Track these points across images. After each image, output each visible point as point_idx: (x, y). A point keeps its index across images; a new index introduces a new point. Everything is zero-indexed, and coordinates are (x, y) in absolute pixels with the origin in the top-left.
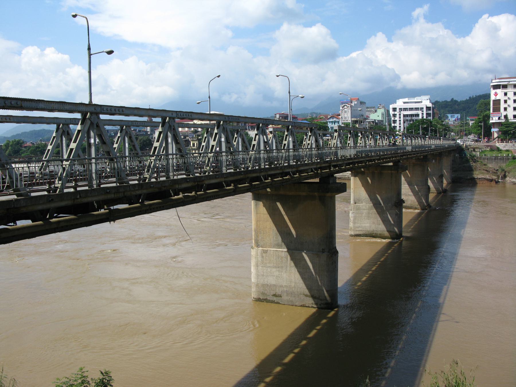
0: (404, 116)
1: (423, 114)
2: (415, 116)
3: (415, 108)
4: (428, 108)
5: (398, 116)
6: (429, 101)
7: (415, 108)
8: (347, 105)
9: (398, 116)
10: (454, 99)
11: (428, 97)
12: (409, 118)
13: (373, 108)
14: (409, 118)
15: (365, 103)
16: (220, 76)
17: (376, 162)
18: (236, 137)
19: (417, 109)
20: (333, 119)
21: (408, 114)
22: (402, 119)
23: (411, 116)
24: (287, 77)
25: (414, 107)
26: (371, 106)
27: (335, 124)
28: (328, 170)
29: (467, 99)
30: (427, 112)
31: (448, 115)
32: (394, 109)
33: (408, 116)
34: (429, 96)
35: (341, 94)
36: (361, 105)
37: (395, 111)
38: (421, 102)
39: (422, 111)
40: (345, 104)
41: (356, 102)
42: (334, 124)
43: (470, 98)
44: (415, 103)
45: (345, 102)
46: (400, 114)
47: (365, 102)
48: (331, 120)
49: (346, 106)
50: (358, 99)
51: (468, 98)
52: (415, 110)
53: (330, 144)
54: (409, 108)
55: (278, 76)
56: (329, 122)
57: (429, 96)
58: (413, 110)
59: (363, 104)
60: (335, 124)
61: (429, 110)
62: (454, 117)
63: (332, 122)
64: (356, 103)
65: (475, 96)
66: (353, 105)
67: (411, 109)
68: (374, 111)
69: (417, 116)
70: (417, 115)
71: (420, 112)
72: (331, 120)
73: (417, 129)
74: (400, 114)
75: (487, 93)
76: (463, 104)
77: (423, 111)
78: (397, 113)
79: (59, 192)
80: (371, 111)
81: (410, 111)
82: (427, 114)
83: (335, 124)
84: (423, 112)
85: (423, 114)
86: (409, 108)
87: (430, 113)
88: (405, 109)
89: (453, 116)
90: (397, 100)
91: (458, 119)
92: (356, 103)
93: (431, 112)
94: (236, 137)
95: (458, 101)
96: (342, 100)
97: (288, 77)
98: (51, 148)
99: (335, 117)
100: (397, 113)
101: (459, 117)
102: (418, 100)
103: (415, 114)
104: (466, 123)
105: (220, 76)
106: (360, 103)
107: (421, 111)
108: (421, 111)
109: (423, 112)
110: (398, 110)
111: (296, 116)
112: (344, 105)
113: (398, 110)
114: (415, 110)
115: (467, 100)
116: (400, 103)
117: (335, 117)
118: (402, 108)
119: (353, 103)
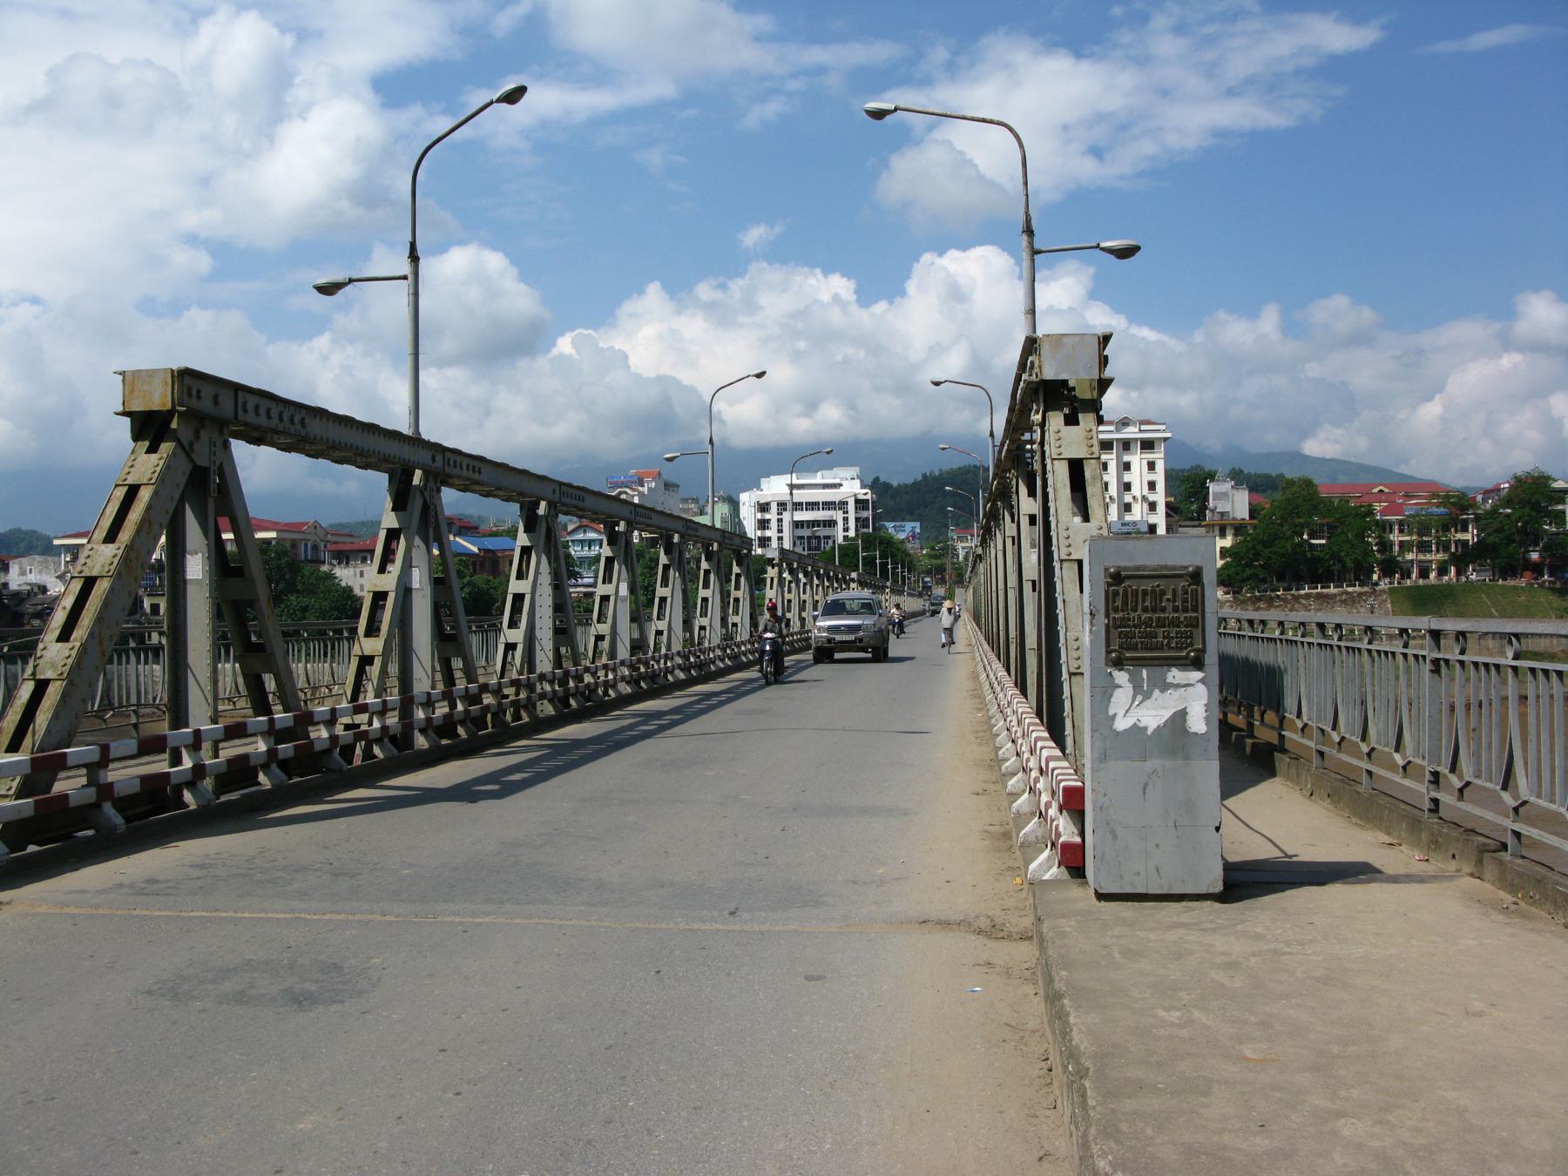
0: (797, 525)
1: (846, 520)
2: (825, 526)
3: (823, 503)
4: (861, 504)
5: (774, 525)
6: (857, 482)
7: (823, 503)
8: (628, 490)
9: (774, 525)
10: (882, 479)
11: (854, 471)
12: (806, 532)
13: (696, 501)
14: (806, 532)
15: (678, 486)
16: (763, 373)
17: (795, 637)
18: (664, 565)
19: (828, 505)
20: (585, 532)
21: (803, 521)
22: (786, 534)
23: (802, 527)
24: (979, 386)
25: (821, 500)
26: (686, 497)
27: (590, 548)
28: (867, 652)
29: (916, 479)
30: (858, 516)
31: (886, 524)
32: (764, 507)
33: (802, 527)
34: (858, 469)
35: (944, 449)
36: (667, 492)
37: (764, 511)
38: (841, 485)
39: (844, 513)
40: (621, 487)
41: (654, 484)
42: (587, 548)
43: (924, 476)
44: (824, 489)
45: (623, 482)
46: (780, 521)
47: (678, 483)
48: (580, 536)
49: (626, 493)
50: (659, 474)
51: (920, 478)
52: (823, 509)
53: (519, 598)
54: (806, 503)
55: (937, 384)
56: (573, 541)
57: (858, 469)
58: (819, 509)
59: (671, 489)
60: (593, 548)
61: (863, 510)
62: (904, 531)
63: (582, 542)
64: (653, 485)
65: (937, 474)
66: (646, 493)
67: (812, 506)
68: (695, 510)
69: (830, 526)
70: (831, 523)
71: (838, 516)
72: (580, 536)
73: (852, 564)
74: (780, 521)
75: (970, 465)
76: (907, 493)
77: (847, 512)
78: (772, 516)
79: (98, 707)
80: (688, 509)
81: (810, 512)
82: (857, 519)
83: (590, 548)
84: (846, 515)
85: (846, 520)
86: (806, 503)
87: (867, 519)
88: (797, 506)
89: (900, 526)
90: (762, 480)
91: (913, 537)
92: (653, 485)
93: (869, 514)
94: (664, 565)
95: (892, 486)
96: (613, 477)
97: (983, 389)
98: (393, 587)
99: (592, 528)
100: (772, 516)
101: (918, 530)
102: (826, 478)
103: (807, 521)
104: (945, 549)
105: (763, 373)
106: (665, 485)
107: (841, 512)
108: (841, 512)
109: (846, 515)
110: (774, 507)
111: (474, 522)
112: (619, 490)
113: (774, 507)
114: (823, 509)
115: (915, 483)
116: (776, 487)
117: (592, 528)
118: (817, 500)
119: (646, 485)
